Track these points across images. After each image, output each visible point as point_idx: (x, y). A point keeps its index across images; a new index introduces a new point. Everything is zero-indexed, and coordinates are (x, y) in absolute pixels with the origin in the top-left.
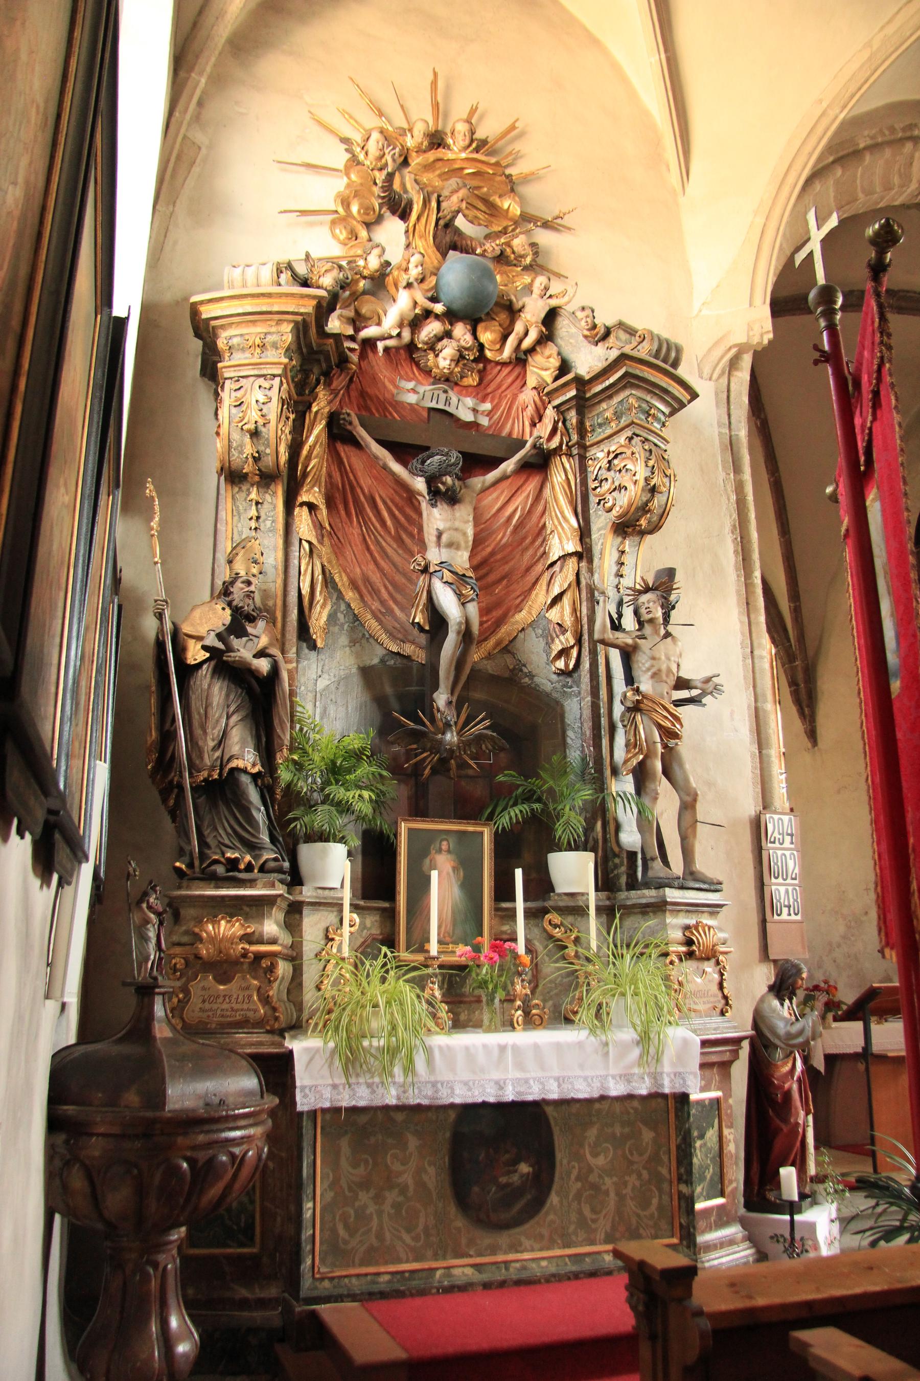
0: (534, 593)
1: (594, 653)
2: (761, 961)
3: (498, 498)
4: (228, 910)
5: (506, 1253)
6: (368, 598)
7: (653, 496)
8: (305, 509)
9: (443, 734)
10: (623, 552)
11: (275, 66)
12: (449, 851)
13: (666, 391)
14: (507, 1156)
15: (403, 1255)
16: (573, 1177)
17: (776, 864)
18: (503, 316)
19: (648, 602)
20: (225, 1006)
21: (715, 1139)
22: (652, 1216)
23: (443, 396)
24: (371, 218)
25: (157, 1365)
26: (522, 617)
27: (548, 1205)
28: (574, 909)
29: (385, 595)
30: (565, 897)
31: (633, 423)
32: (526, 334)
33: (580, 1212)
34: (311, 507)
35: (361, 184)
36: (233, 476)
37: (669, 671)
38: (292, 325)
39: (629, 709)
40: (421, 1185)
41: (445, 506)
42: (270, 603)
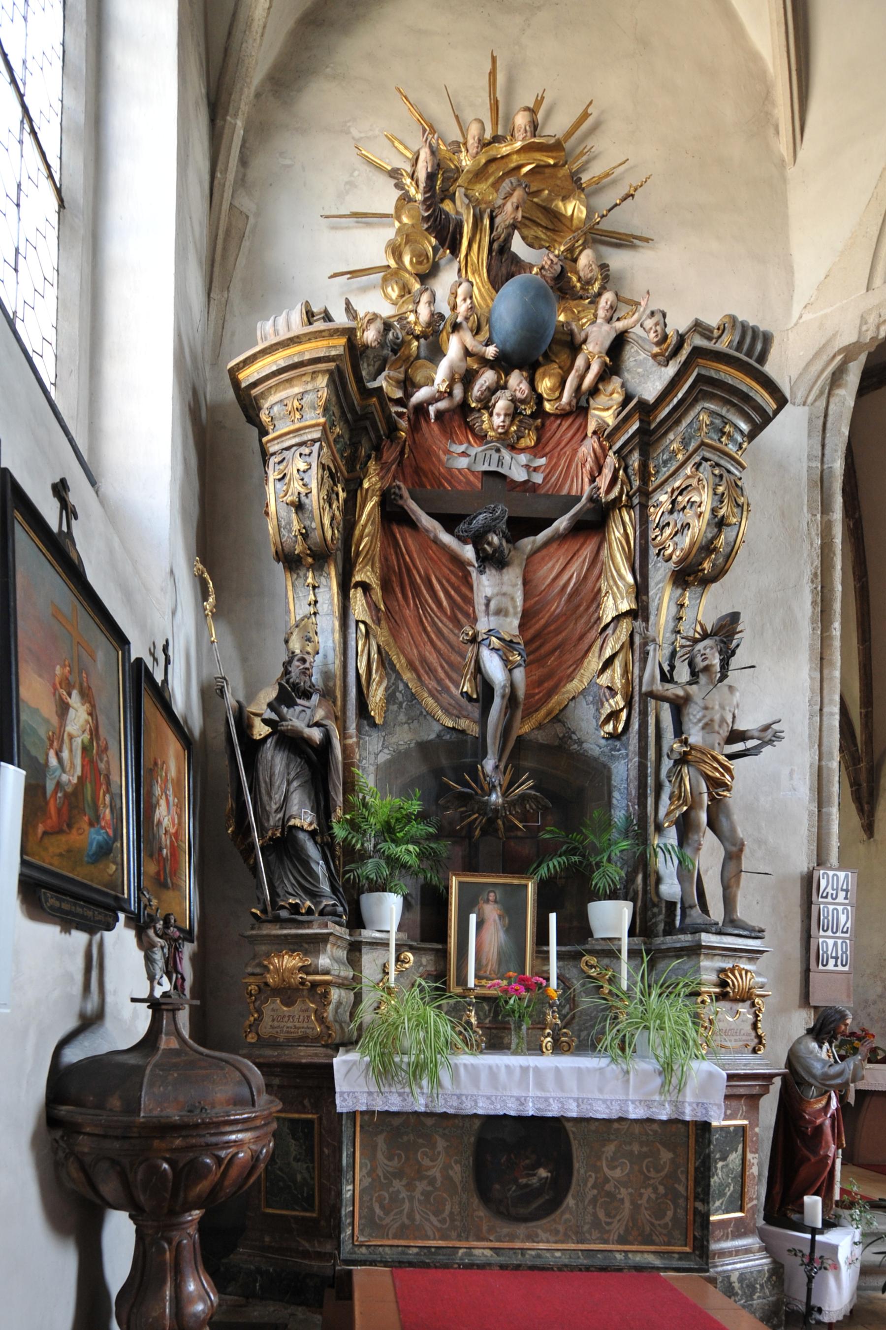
0: (586, 661)
1: (644, 714)
2: (800, 1007)
3: (553, 566)
4: (291, 947)
5: (523, 1241)
6: (425, 677)
7: (720, 531)
8: (360, 591)
9: (490, 795)
10: (682, 605)
11: (321, 97)
12: (495, 902)
13: (746, 398)
14: (527, 1161)
15: (430, 1233)
16: (590, 1185)
17: (827, 918)
18: (564, 357)
19: (705, 648)
20: (289, 1024)
21: (738, 1162)
22: (666, 1226)
23: (495, 456)
24: (424, 268)
25: (168, 1323)
26: (575, 685)
27: (564, 1205)
28: (609, 952)
29: (442, 675)
30: (602, 942)
31: (703, 444)
32: (588, 367)
33: (595, 1215)
34: (366, 587)
35: (413, 226)
36: (291, 562)
37: (723, 720)
38: (326, 377)
39: (677, 763)
40: (448, 1178)
41: (494, 571)
42: (331, 684)
